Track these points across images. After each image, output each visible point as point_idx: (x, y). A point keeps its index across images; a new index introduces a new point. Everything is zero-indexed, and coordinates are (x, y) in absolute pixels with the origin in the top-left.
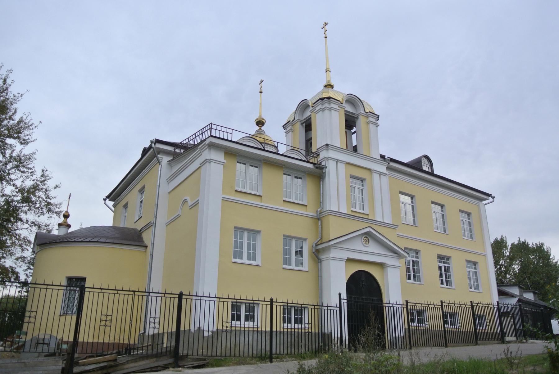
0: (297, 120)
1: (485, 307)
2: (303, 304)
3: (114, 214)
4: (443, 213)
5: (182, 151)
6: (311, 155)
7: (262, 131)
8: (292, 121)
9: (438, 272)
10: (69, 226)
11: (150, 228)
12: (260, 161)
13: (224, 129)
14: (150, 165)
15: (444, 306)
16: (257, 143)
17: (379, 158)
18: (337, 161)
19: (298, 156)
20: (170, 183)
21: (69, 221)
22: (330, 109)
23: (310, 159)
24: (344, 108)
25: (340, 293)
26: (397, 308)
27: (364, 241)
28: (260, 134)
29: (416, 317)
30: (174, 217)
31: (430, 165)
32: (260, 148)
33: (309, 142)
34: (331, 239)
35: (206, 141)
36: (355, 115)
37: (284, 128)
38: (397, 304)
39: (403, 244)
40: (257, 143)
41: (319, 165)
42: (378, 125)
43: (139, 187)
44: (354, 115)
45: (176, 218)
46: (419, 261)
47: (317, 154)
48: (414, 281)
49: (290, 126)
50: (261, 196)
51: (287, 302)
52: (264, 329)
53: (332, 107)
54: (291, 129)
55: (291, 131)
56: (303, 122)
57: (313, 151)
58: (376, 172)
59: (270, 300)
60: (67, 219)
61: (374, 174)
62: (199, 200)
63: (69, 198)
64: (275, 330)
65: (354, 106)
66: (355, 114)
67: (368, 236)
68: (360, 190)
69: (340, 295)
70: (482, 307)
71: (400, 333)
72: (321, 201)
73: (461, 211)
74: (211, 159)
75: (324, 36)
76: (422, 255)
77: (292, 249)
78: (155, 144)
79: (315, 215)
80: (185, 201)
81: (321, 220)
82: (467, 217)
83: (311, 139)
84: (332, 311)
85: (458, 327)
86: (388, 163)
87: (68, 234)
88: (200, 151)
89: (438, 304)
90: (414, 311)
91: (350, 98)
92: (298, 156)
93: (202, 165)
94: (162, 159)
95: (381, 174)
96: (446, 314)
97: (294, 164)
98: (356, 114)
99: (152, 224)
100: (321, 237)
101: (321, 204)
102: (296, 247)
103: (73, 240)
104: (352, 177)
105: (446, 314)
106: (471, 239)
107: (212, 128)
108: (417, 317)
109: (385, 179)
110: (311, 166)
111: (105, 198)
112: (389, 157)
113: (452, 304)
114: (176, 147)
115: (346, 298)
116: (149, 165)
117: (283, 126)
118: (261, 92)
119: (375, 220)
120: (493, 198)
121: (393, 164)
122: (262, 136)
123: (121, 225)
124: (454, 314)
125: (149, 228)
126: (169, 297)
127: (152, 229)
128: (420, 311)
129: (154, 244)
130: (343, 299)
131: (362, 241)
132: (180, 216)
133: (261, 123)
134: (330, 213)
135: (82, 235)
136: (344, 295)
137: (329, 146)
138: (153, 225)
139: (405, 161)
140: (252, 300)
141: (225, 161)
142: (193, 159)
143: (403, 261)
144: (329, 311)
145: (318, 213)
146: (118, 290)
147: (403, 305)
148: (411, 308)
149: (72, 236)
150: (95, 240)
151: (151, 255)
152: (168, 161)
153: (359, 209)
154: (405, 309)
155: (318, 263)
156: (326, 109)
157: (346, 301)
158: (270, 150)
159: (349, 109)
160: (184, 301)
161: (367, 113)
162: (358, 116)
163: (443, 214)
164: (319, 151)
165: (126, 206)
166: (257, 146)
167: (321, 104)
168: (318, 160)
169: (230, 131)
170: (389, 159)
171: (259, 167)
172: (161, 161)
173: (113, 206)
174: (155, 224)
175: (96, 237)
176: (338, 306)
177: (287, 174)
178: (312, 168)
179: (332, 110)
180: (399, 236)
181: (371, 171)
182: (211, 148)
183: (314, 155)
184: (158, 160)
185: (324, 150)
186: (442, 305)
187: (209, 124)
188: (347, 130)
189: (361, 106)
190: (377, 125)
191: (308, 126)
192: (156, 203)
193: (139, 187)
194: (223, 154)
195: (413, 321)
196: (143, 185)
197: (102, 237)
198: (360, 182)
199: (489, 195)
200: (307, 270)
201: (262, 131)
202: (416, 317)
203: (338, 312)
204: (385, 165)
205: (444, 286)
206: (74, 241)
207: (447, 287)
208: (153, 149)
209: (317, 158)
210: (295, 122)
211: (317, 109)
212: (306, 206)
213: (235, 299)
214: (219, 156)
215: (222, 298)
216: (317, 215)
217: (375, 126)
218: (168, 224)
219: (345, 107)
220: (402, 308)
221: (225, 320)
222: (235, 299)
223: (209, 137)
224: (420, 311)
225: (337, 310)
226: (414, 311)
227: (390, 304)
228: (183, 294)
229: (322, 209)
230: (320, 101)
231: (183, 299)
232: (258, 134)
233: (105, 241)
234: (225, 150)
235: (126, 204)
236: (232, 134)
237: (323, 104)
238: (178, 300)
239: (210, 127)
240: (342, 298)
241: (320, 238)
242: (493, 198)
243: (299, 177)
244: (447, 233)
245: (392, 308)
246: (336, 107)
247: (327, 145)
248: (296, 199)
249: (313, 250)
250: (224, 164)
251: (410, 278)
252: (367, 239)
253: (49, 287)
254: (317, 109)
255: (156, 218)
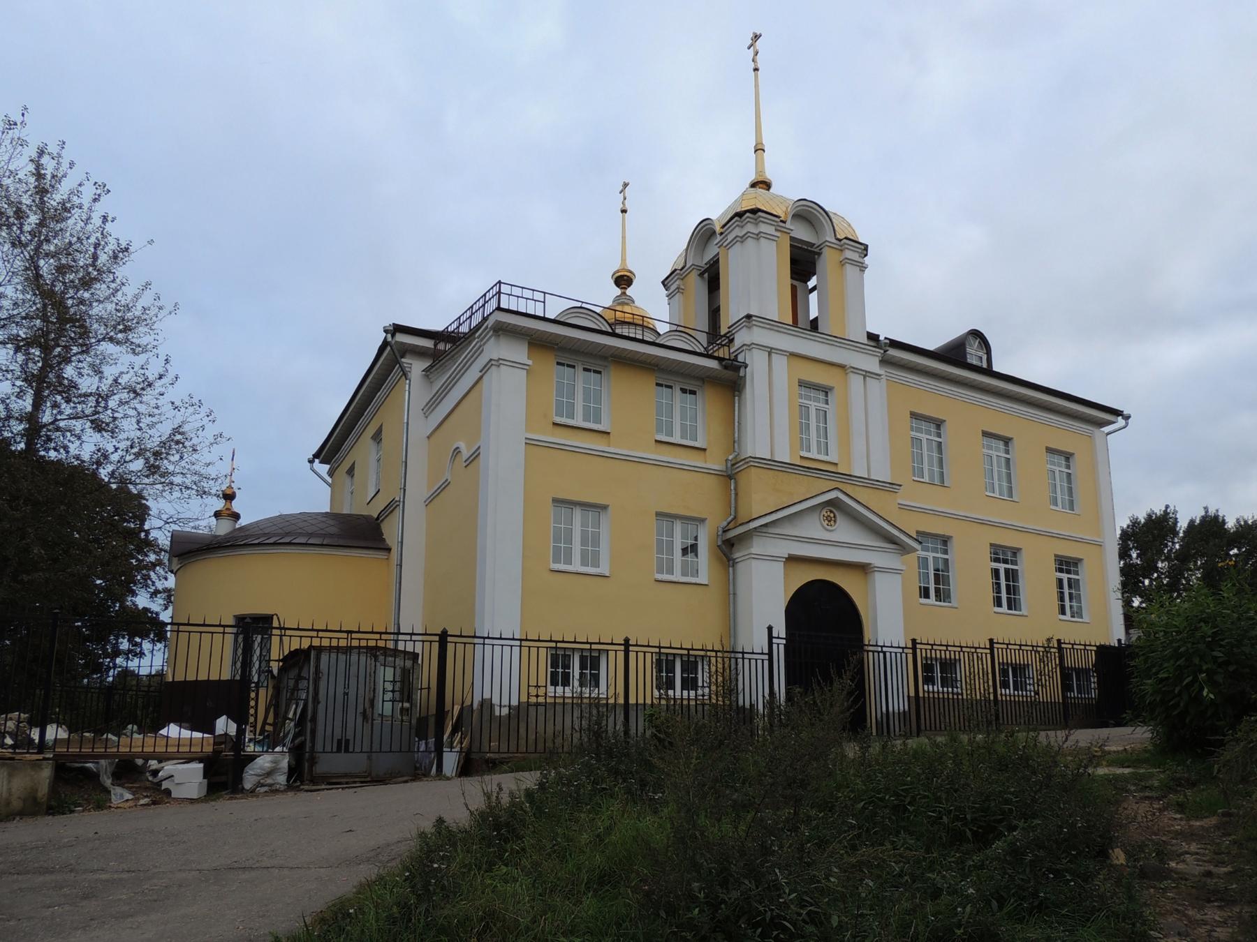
0: (689, 268)
1: (1089, 652)
2: (693, 649)
3: (332, 489)
4: (1008, 456)
5: (448, 346)
6: (718, 342)
7: (628, 298)
8: (681, 270)
9: (989, 580)
10: (236, 517)
11: (395, 511)
12: (604, 358)
13: (528, 294)
14: (389, 382)
15: (996, 650)
16: (597, 319)
17: (865, 340)
18: (771, 351)
19: (687, 343)
20: (432, 415)
21: (236, 506)
22: (758, 236)
23: (714, 352)
24: (789, 233)
25: (770, 625)
26: (893, 655)
27: (824, 520)
28: (623, 304)
29: (938, 674)
30: (438, 486)
31: (985, 352)
32: (604, 329)
33: (714, 313)
34: (754, 517)
35: (487, 322)
36: (815, 246)
37: (665, 286)
38: (892, 647)
39: (913, 524)
40: (597, 319)
41: (730, 362)
42: (866, 268)
43: (371, 431)
44: (812, 247)
45: (442, 488)
46: (1019, 571)
47: (728, 337)
48: (936, 600)
49: (676, 281)
50: (609, 433)
51: (658, 645)
52: (641, 701)
53: (761, 232)
54: (678, 288)
55: (678, 292)
56: (703, 269)
57: (722, 333)
58: (856, 370)
59: (623, 642)
60: (231, 503)
61: (852, 375)
62: (479, 448)
63: (233, 459)
64: (643, 702)
65: (813, 226)
66: (814, 244)
67: (834, 508)
68: (822, 413)
69: (770, 629)
70: (1083, 651)
71: (898, 703)
72: (736, 439)
73: (1050, 450)
74: (500, 359)
75: (752, 65)
76: (954, 546)
77: (674, 541)
78: (393, 336)
79: (723, 468)
80: (457, 451)
81: (735, 479)
82: (1064, 463)
83: (719, 310)
84: (753, 662)
85: (970, 682)
86: (882, 351)
87: (235, 530)
88: (478, 344)
89: (982, 646)
90: (934, 662)
91: (804, 208)
92: (687, 343)
93: (483, 372)
94: (411, 368)
95: (867, 374)
96: (1006, 667)
97: (653, 355)
98: (815, 246)
99: (398, 503)
100: (735, 513)
101: (736, 445)
102: (684, 536)
103: (242, 543)
104: (802, 384)
105: (1006, 667)
106: (1070, 510)
107: (502, 291)
108: (939, 675)
109: (877, 389)
110: (712, 364)
111: (312, 457)
112: (887, 337)
113: (1015, 644)
114: (438, 339)
115: (783, 635)
116: (387, 381)
117: (663, 282)
118: (624, 211)
119: (852, 474)
120: (1127, 418)
121: (894, 353)
122: (627, 309)
123: (346, 511)
124: (1022, 666)
125: (392, 512)
126: (186, 632)
127: (398, 512)
128: (948, 662)
129: (402, 542)
130: (775, 638)
131: (820, 519)
132: (450, 482)
133: (624, 280)
134: (752, 464)
135: (261, 532)
136: (780, 629)
137: (754, 318)
138: (399, 505)
139: (931, 346)
140: (587, 643)
141: (530, 362)
142: (467, 362)
143: (912, 558)
144: (746, 661)
145: (729, 465)
146: (318, 631)
147: (906, 648)
148: (924, 655)
149: (243, 534)
150: (287, 540)
151: (398, 566)
152: (423, 371)
153: (818, 453)
154: (910, 657)
155: (729, 567)
156: (749, 236)
157: (784, 642)
158: (627, 334)
159: (802, 233)
160: (450, 647)
161: (840, 240)
162: (821, 249)
163: (1009, 459)
164: (733, 332)
165: (351, 471)
166: (599, 326)
167: (737, 225)
168: (731, 351)
169: (539, 296)
170: (887, 341)
171: (576, 367)
172: (410, 372)
173: (328, 473)
174: (404, 502)
175: (287, 534)
176: (766, 651)
177: (566, 362)
178: (717, 369)
179: (762, 239)
180: (902, 507)
181: (846, 370)
182: (499, 336)
183: (722, 341)
184: (402, 370)
185: (743, 327)
186: (992, 648)
187: (496, 285)
188: (796, 280)
189: (828, 225)
190: (862, 267)
191: (712, 277)
192: (404, 460)
193: (371, 431)
194: (527, 344)
195: (1005, 685)
196: (378, 426)
197: (301, 534)
198: (1001, 445)
199: (1117, 413)
200: (706, 583)
201: (628, 298)
202: (938, 674)
203: (766, 663)
204: (877, 356)
205: (1004, 609)
206: (244, 545)
207: (1010, 612)
208: (391, 347)
209: (729, 346)
210: (686, 271)
211: (730, 238)
212: (704, 450)
213: (554, 641)
214: (517, 352)
215: (527, 640)
216: (727, 468)
217: (858, 268)
218: (429, 501)
219: (792, 230)
220: (904, 655)
221: (533, 683)
222: (554, 641)
223: (493, 311)
224: (948, 662)
225: (763, 660)
226: (934, 662)
227: (877, 646)
228: (448, 633)
229: (739, 454)
230: (736, 218)
231: (448, 644)
232: (619, 304)
233: (304, 542)
234: (529, 338)
235: (351, 467)
236: (544, 302)
237: (742, 227)
238: (440, 647)
239: (498, 290)
240: (775, 634)
241: (732, 517)
242: (1127, 418)
243: (690, 390)
244: (1015, 498)
245: (881, 655)
246: (770, 230)
247: (749, 317)
248: (586, 419)
249: (717, 541)
250: (527, 368)
251: (1000, 605)
252: (832, 515)
253: (181, 628)
254: (730, 238)
255: (405, 490)
